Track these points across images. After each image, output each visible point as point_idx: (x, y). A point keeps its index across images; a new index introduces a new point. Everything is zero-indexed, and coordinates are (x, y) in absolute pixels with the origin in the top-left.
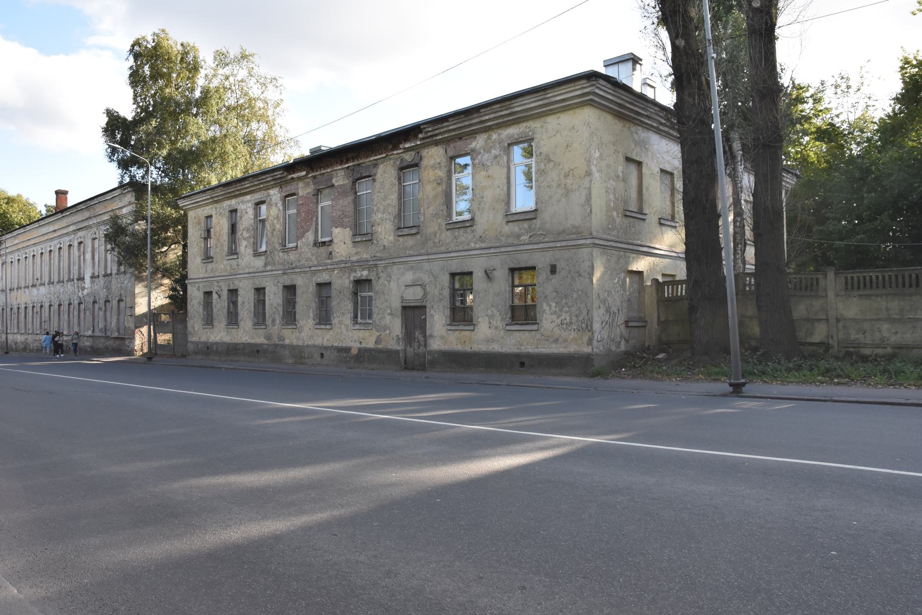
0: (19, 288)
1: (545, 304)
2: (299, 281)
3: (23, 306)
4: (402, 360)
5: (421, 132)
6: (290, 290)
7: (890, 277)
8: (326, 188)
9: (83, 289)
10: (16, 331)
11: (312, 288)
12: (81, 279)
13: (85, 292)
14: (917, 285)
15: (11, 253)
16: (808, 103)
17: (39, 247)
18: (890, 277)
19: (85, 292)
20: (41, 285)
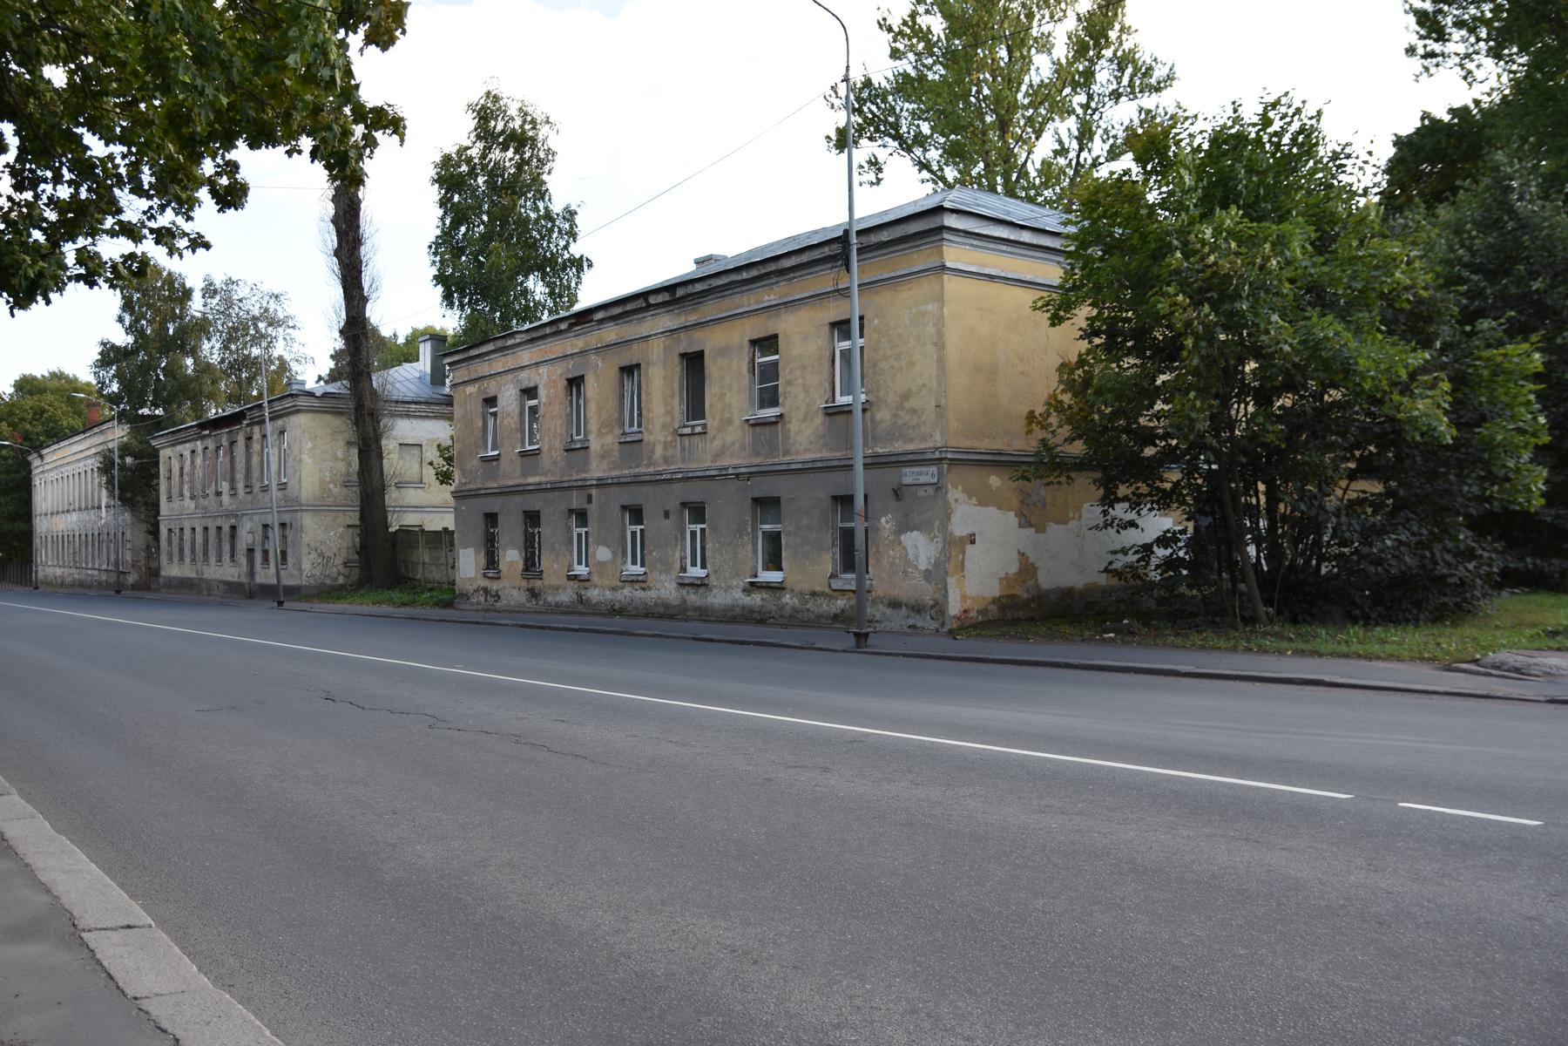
0: (58, 513)
1: (1137, 361)
2: (210, 525)
3: (60, 534)
4: (248, 591)
5: (245, 418)
6: (206, 529)
7: (631, 425)
8: (513, 625)
9: (101, 518)
10: (90, 566)
11: (214, 528)
12: (99, 508)
13: (103, 522)
14: (879, 22)
15: (51, 470)
16: (276, 310)
17: (69, 468)
18: (631, 425)
19: (103, 522)
20: (74, 510)
